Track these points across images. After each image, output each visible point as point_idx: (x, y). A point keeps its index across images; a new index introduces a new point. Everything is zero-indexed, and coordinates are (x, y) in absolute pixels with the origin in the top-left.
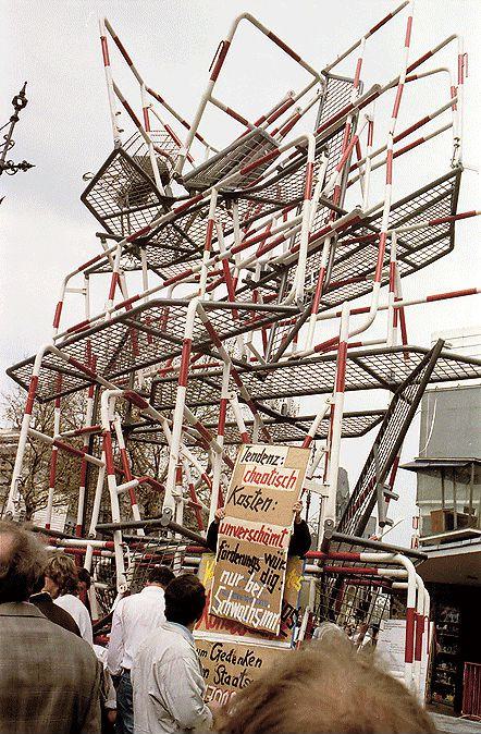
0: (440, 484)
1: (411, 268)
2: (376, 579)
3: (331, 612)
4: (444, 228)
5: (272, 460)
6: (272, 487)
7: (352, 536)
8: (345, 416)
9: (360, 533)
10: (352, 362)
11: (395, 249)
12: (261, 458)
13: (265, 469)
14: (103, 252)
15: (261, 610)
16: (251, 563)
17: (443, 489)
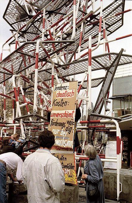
0: (120, 103)
1: (110, 33)
2: (105, 129)
3: (92, 140)
4: (119, 17)
5: (65, 88)
6: (67, 97)
7: (98, 114)
8: (92, 80)
9: (100, 113)
10: (93, 60)
11: (105, 26)
12: (60, 88)
13: (63, 91)
14: (13, 35)
15: (67, 141)
16: (62, 125)
17: (121, 103)
